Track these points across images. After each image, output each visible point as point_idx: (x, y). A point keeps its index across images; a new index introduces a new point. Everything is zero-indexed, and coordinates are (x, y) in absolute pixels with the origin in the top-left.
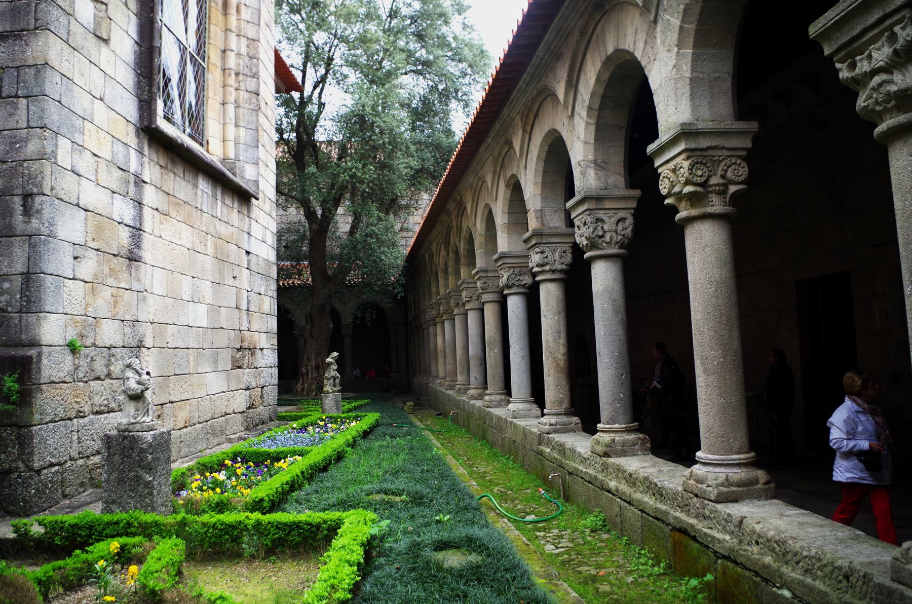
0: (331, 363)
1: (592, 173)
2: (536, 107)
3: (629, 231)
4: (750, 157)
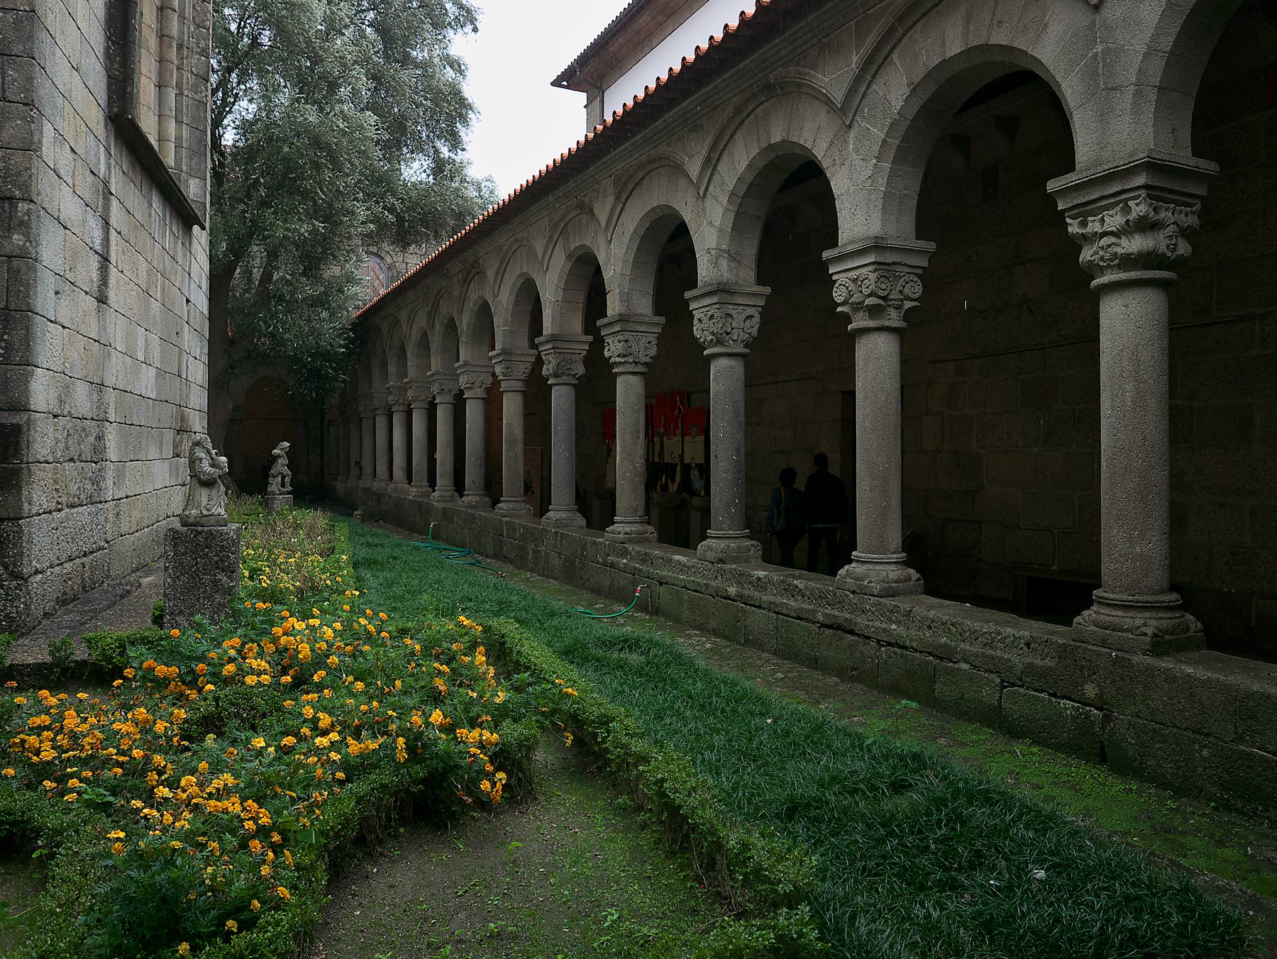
0: (279, 456)
1: (724, 263)
2: (640, 175)
3: (754, 331)
4: (925, 276)
